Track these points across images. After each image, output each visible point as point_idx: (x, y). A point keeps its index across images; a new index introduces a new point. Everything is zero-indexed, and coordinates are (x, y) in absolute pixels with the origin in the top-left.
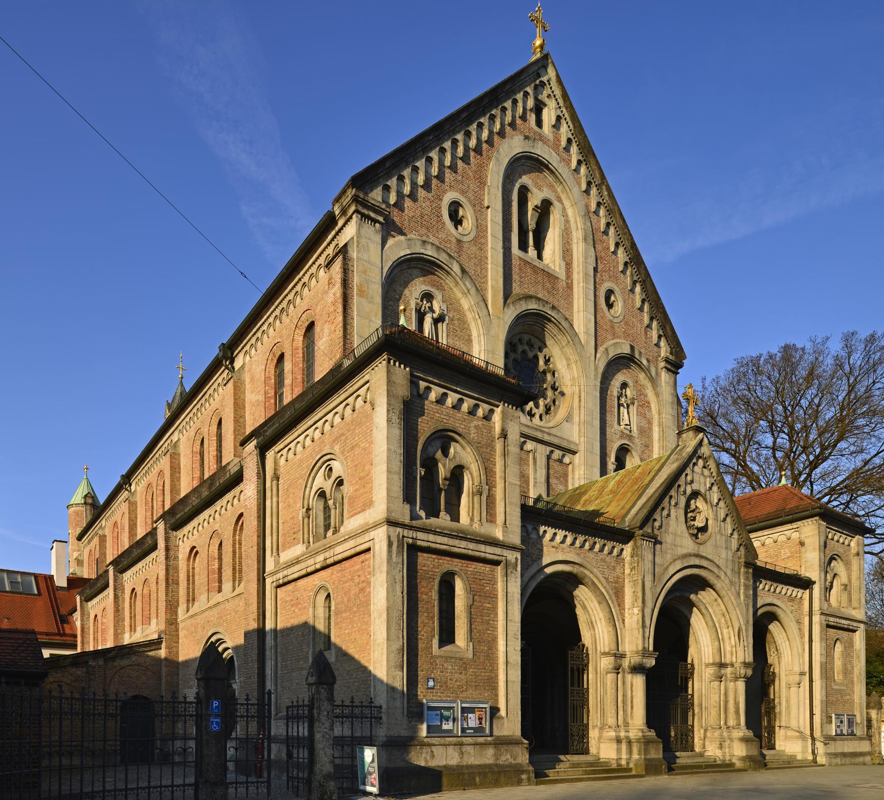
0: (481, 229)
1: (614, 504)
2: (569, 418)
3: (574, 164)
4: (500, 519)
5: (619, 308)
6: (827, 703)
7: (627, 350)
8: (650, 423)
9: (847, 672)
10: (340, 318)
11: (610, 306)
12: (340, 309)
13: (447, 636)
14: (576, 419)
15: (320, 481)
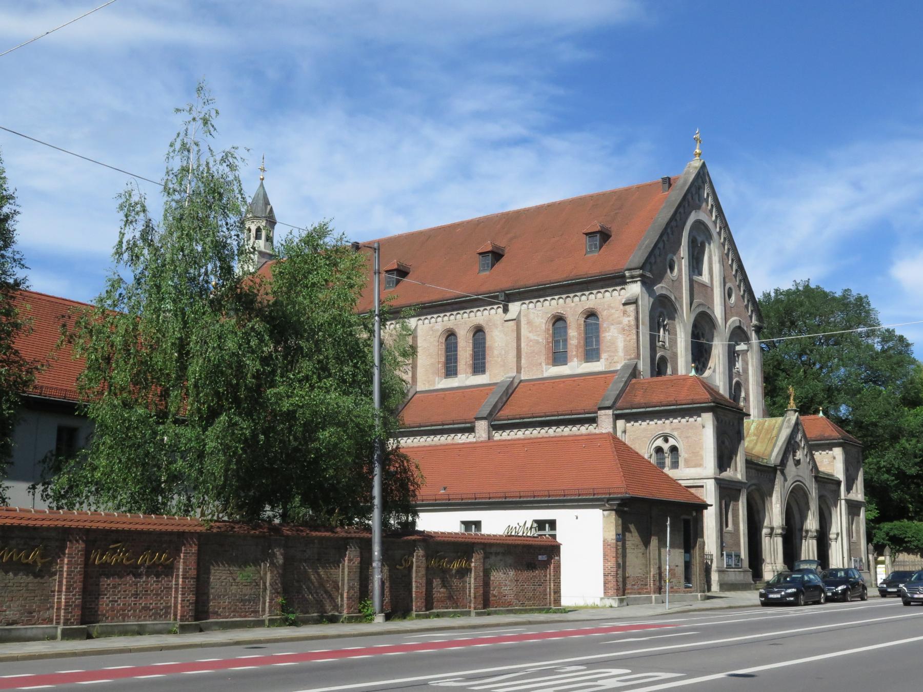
0: (680, 270)
1: (759, 444)
2: (714, 371)
3: (714, 218)
4: (739, 469)
5: (733, 298)
6: (850, 550)
7: (738, 324)
8: (747, 364)
9: (858, 532)
10: (635, 337)
11: (730, 296)
12: (634, 331)
13: (727, 526)
14: (717, 371)
15: (660, 442)
